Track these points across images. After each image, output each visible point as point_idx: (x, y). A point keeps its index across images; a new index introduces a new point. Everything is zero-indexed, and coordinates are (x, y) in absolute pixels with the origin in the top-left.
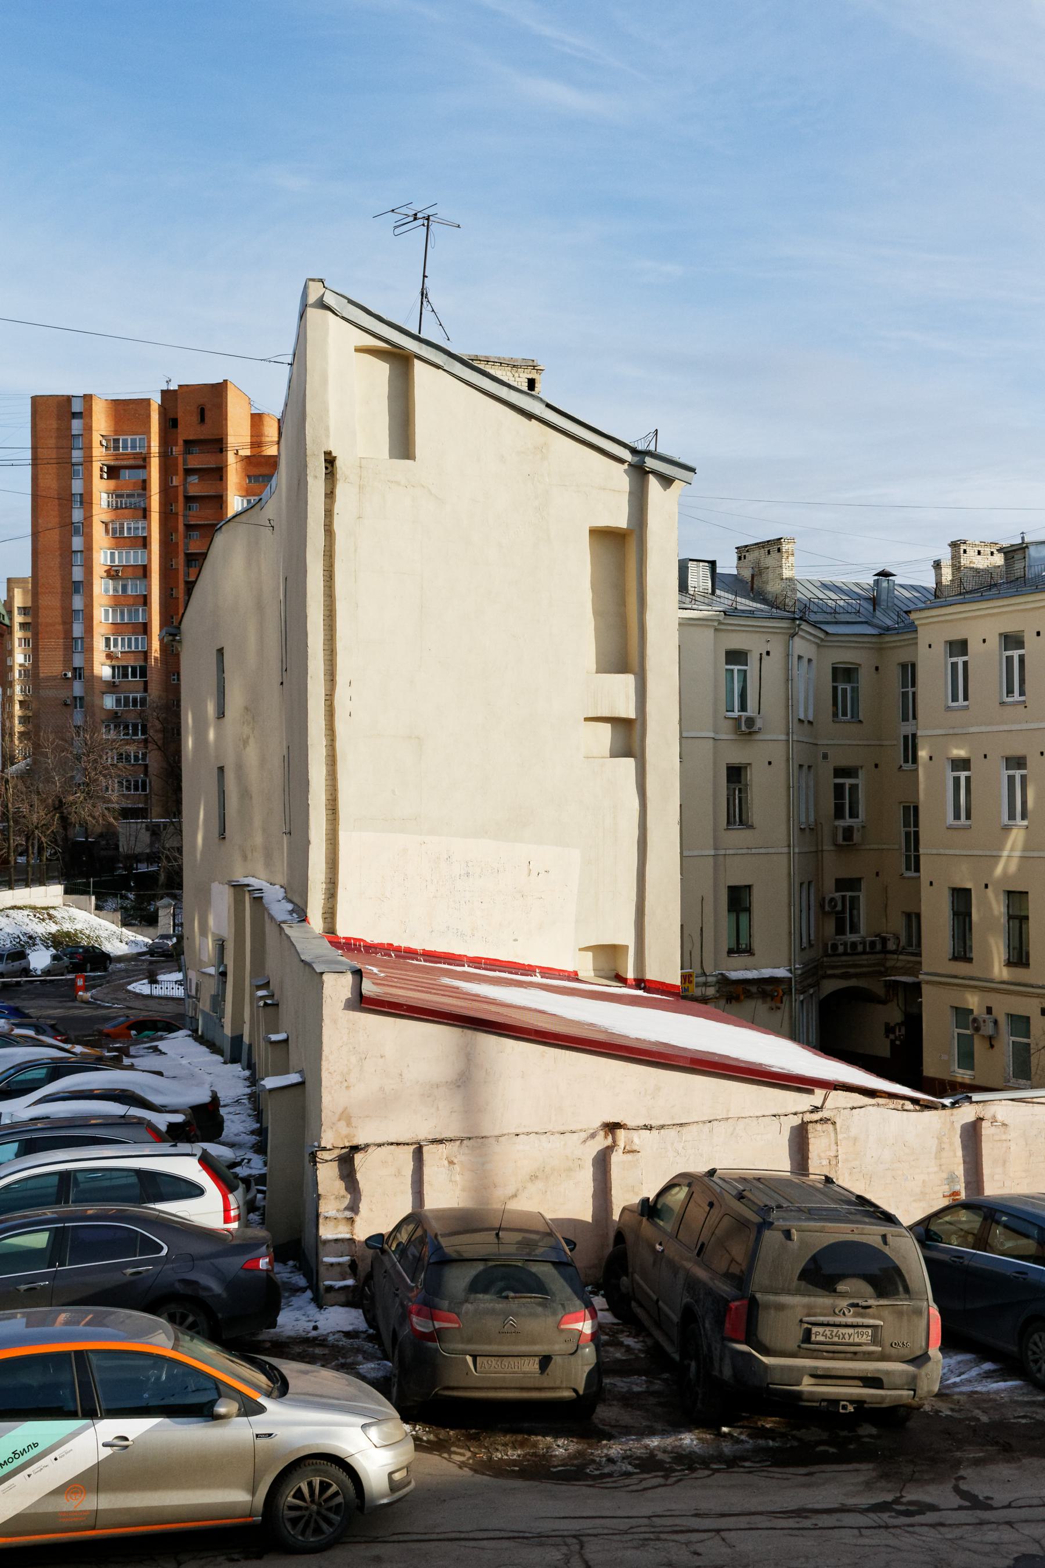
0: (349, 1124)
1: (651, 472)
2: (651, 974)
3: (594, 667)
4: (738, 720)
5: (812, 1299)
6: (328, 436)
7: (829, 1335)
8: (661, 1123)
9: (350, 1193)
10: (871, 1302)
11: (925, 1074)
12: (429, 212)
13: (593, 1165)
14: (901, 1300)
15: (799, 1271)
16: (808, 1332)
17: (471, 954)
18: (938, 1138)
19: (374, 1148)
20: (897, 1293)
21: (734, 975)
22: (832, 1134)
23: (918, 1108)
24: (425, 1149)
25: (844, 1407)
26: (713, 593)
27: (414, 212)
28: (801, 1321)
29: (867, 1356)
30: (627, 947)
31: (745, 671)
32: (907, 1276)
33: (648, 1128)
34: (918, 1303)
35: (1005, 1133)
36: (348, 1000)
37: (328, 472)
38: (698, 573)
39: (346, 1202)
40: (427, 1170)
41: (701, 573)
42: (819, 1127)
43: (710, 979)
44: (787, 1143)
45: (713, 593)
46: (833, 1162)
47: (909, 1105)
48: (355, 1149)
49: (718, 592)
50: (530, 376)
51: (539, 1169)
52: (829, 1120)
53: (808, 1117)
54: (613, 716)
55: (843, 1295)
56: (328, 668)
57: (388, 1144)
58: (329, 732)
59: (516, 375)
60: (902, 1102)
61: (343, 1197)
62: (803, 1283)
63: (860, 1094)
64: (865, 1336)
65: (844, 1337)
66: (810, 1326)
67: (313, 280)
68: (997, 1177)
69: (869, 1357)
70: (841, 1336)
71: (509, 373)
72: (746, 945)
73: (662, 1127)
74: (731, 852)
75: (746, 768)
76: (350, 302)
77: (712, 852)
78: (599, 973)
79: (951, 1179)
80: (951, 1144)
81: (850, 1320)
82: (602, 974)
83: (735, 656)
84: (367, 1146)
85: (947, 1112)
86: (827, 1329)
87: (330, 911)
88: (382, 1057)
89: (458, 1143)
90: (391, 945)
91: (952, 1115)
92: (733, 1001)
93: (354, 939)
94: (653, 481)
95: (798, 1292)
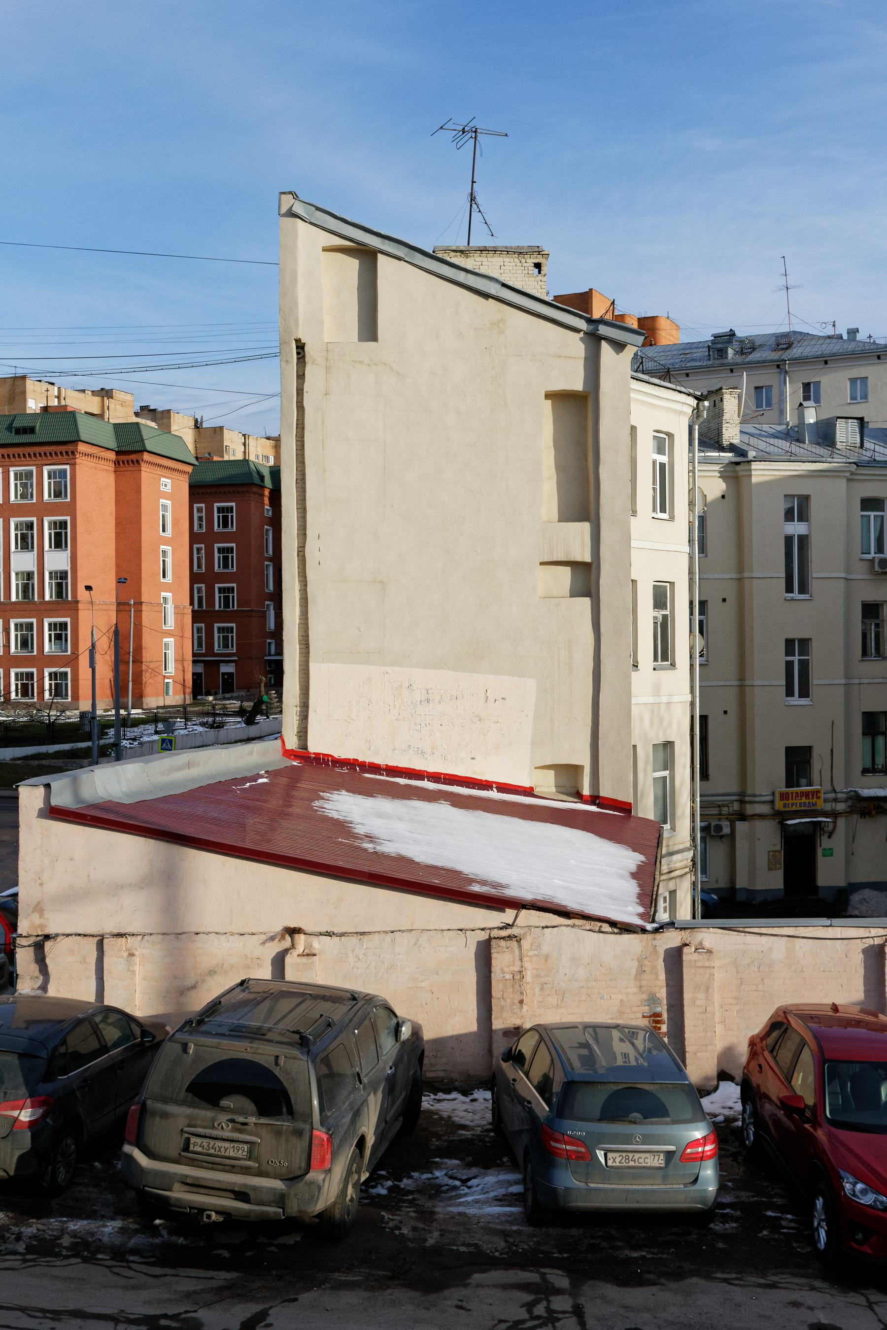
0: (41, 916)
1: (604, 339)
2: (605, 792)
3: (555, 516)
4: (872, 561)
5: (196, 1111)
6: (297, 326)
7: (206, 1146)
8: (344, 930)
9: (43, 975)
10: (252, 1120)
11: (737, 899)
12: (471, 125)
13: (272, 964)
14: (284, 1121)
15: (188, 1084)
16: (188, 1141)
17: (431, 769)
18: (638, 961)
19: (63, 937)
20: (280, 1113)
21: (866, 793)
22: (517, 951)
23: (616, 930)
24: (105, 941)
25: (209, 1217)
26: (862, 446)
27: (462, 128)
28: (182, 1130)
29: (244, 1170)
30: (582, 767)
31: (882, 517)
32: (292, 1098)
33: (329, 934)
34: (301, 1125)
35: (708, 960)
36: (40, 810)
37: (299, 356)
38: (847, 428)
39: (39, 982)
40: (107, 960)
41: (850, 429)
42: (503, 943)
43: (840, 796)
44: (473, 956)
45: (862, 446)
46: (518, 977)
47: (606, 927)
48: (47, 937)
49: (867, 445)
50: (536, 261)
51: (217, 965)
52: (516, 937)
53: (495, 933)
54: (568, 560)
55: (226, 1110)
56: (302, 524)
57: (76, 935)
58: (302, 579)
59: (523, 261)
60: (599, 924)
61: (37, 977)
62: (190, 1095)
63: (554, 914)
64: (240, 1151)
65: (220, 1150)
66: (190, 1136)
67: (284, 193)
68: (698, 1002)
69: (246, 1171)
70: (217, 1149)
71: (516, 260)
72: (883, 765)
73: (342, 935)
74: (866, 681)
75: (882, 605)
76: (318, 209)
77: (843, 681)
78: (560, 790)
79: (653, 1000)
80: (654, 968)
81: (227, 1134)
82: (564, 790)
83: (869, 504)
84: (57, 935)
85: (650, 936)
86: (205, 1141)
87: (304, 730)
88: (71, 859)
89: (140, 937)
90: (357, 760)
91: (654, 939)
92: (867, 816)
93: (323, 754)
94: (605, 346)
95: (183, 1103)
